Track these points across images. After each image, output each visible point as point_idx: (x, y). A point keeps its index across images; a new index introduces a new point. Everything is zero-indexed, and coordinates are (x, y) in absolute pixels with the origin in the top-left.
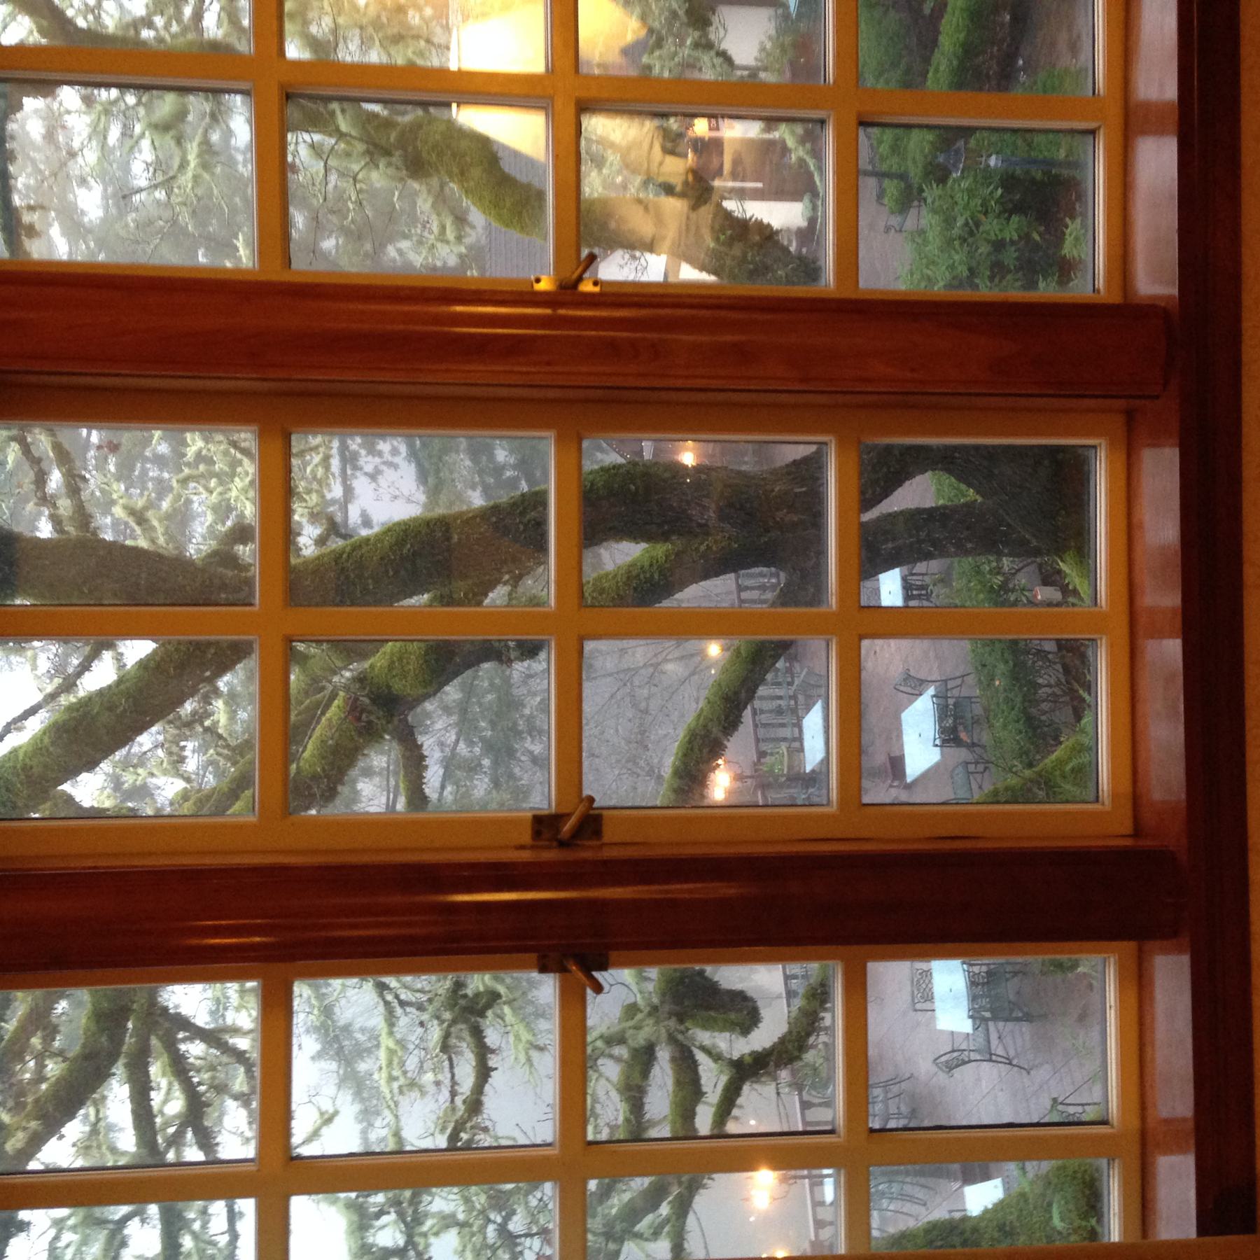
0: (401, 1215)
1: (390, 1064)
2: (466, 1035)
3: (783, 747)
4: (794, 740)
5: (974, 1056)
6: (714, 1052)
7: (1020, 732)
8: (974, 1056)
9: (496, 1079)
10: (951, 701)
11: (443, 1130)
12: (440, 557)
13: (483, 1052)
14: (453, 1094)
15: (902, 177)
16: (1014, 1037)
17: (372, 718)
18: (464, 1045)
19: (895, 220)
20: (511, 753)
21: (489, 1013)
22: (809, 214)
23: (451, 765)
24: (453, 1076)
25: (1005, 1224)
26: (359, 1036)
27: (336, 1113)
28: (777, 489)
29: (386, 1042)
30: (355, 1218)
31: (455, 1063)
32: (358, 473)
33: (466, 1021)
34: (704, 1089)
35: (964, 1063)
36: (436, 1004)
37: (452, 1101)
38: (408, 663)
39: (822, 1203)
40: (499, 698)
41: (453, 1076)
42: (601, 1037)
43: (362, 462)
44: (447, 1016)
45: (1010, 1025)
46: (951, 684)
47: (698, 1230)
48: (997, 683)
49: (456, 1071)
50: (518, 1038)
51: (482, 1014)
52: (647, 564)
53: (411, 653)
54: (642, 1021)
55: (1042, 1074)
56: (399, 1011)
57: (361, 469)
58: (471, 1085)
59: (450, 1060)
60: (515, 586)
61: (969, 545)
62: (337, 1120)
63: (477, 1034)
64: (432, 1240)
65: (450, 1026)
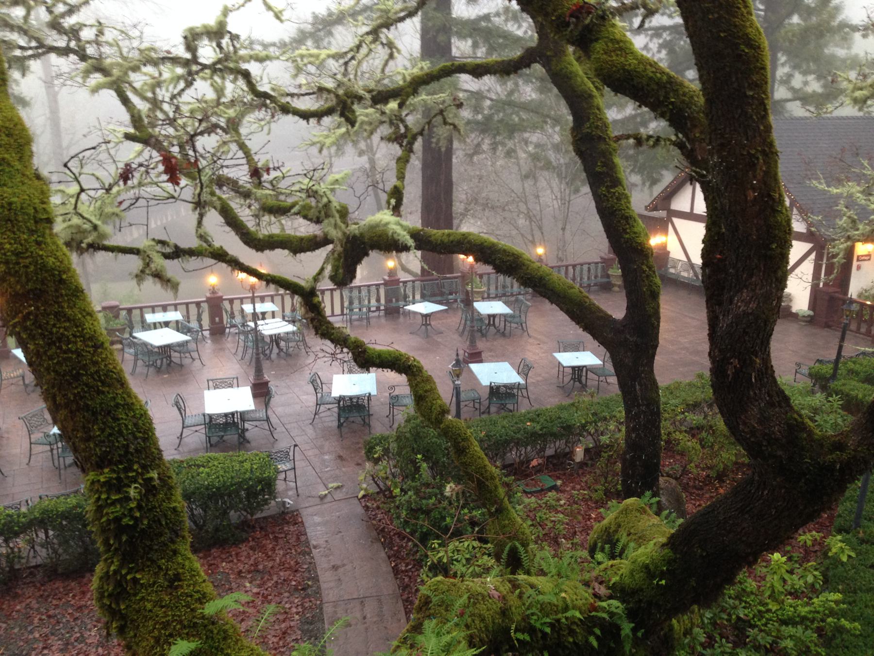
0: (219, 61)
1: (311, 56)
2: (329, 104)
3: (484, 289)
4: (489, 295)
5: (319, 395)
6: (320, 277)
7: (501, 437)
8: (319, 395)
9: (303, 122)
10: (515, 391)
11: (273, 90)
12: (734, 79)
13: (318, 115)
14: (292, 95)
15: (834, 376)
16: (330, 417)
17: (572, 26)
18: (322, 103)
19: (805, 370)
20: (483, 131)
21: (343, 119)
22: (801, 314)
23: (478, 96)
24: (303, 95)
25: (180, 580)
26: (326, 40)
27: (282, 21)
28: (758, 361)
29: (324, 53)
30: (215, 29)
31: (311, 96)
32: (648, 38)
33: (338, 104)
34: (298, 255)
35: (315, 390)
36: (348, 83)
37: (288, 95)
38: (617, 55)
39: (242, 303)
40: (516, 125)
41: (303, 95)
42: (330, 202)
43: (655, 40)
44: (341, 92)
45: (336, 415)
46: (524, 391)
47: (205, 266)
48: (528, 424)
49: (307, 97)
50: (327, 137)
51: (342, 115)
52: (635, 230)
53: (626, 57)
54: (340, 228)
55: (310, 431)
56: (342, 61)
57: (651, 40)
58: (298, 107)
59: (313, 93)
60: (674, 144)
61: (634, 436)
62: (278, 21)
63: (329, 112)
64: (209, 82)
65: (334, 93)
